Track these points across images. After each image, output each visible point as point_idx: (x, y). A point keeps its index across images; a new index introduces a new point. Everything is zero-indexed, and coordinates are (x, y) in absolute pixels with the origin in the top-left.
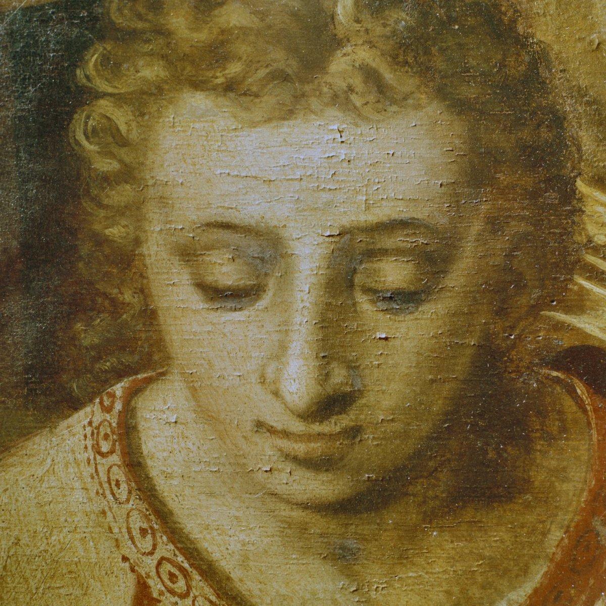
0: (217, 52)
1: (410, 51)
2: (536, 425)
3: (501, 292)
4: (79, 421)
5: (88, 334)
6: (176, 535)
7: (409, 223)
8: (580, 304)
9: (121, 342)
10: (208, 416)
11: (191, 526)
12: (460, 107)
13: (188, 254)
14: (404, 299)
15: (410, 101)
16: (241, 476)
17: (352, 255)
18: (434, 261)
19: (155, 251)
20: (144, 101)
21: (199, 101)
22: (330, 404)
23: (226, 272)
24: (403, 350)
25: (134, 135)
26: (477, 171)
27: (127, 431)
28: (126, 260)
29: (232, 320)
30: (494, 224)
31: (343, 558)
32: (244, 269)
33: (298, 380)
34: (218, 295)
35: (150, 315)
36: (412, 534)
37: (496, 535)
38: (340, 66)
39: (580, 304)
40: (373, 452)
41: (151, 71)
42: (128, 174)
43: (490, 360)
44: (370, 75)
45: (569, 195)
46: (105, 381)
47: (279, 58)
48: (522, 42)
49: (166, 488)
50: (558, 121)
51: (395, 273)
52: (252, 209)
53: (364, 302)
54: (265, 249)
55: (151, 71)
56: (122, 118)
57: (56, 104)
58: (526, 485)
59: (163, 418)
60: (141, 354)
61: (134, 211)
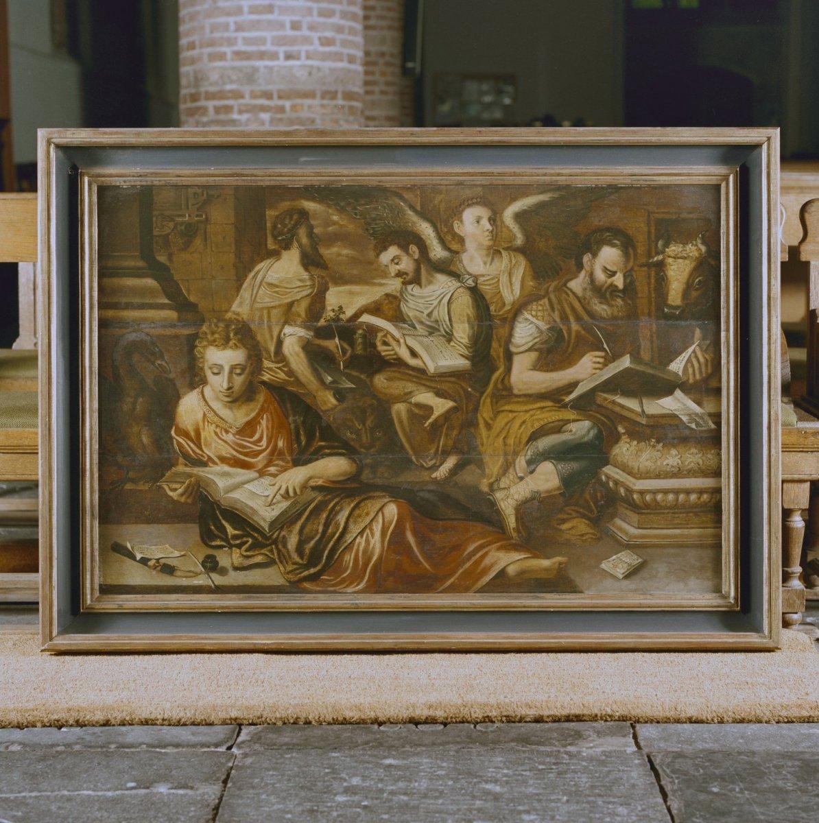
0: (215, 341)
1: (240, 341)
2: (641, 805)
3: (252, 373)
4: (197, 389)
5: (197, 379)
6: (209, 406)
7: (391, 363)
8: (263, 375)
9: (202, 380)
10: (213, 390)
11: (211, 405)
12: (247, 348)
13: (210, 368)
14: (240, 374)
15: (39, 753)
16: (218, 398)
17: (233, 368)
18: (243, 369)
19: (206, 368)
20: (205, 347)
21: (212, 348)
22: (229, 389)
23: (216, 371)
24: (239, 381)
25: (306, 391)
26: (249, 357)
27: (202, 393)
28: (202, 369)
29: (216, 377)
30: (251, 364)
31: (231, 408)
32: (218, 370)
33: (225, 385)
34: (214, 374)
35: (205, 376)
36: (240, 406)
37: (252, 405)
38: (231, 343)
39: (263, 375)
40: (235, 395)
41: (205, 343)
42: (202, 358)
43: (251, 382)
44: (235, 344)
45: (261, 360)
46: (198, 386)
47: (223, 342)
48: (255, 340)
49: (208, 400)
50: (260, 351)
51: (238, 371)
52: (220, 362)
53: (234, 375)
54: (221, 367)
55: (205, 343)
56: (201, 350)
57: (192, 347)
58: (255, 399)
59: (208, 391)
60: (204, 382)
61: (203, 362)
